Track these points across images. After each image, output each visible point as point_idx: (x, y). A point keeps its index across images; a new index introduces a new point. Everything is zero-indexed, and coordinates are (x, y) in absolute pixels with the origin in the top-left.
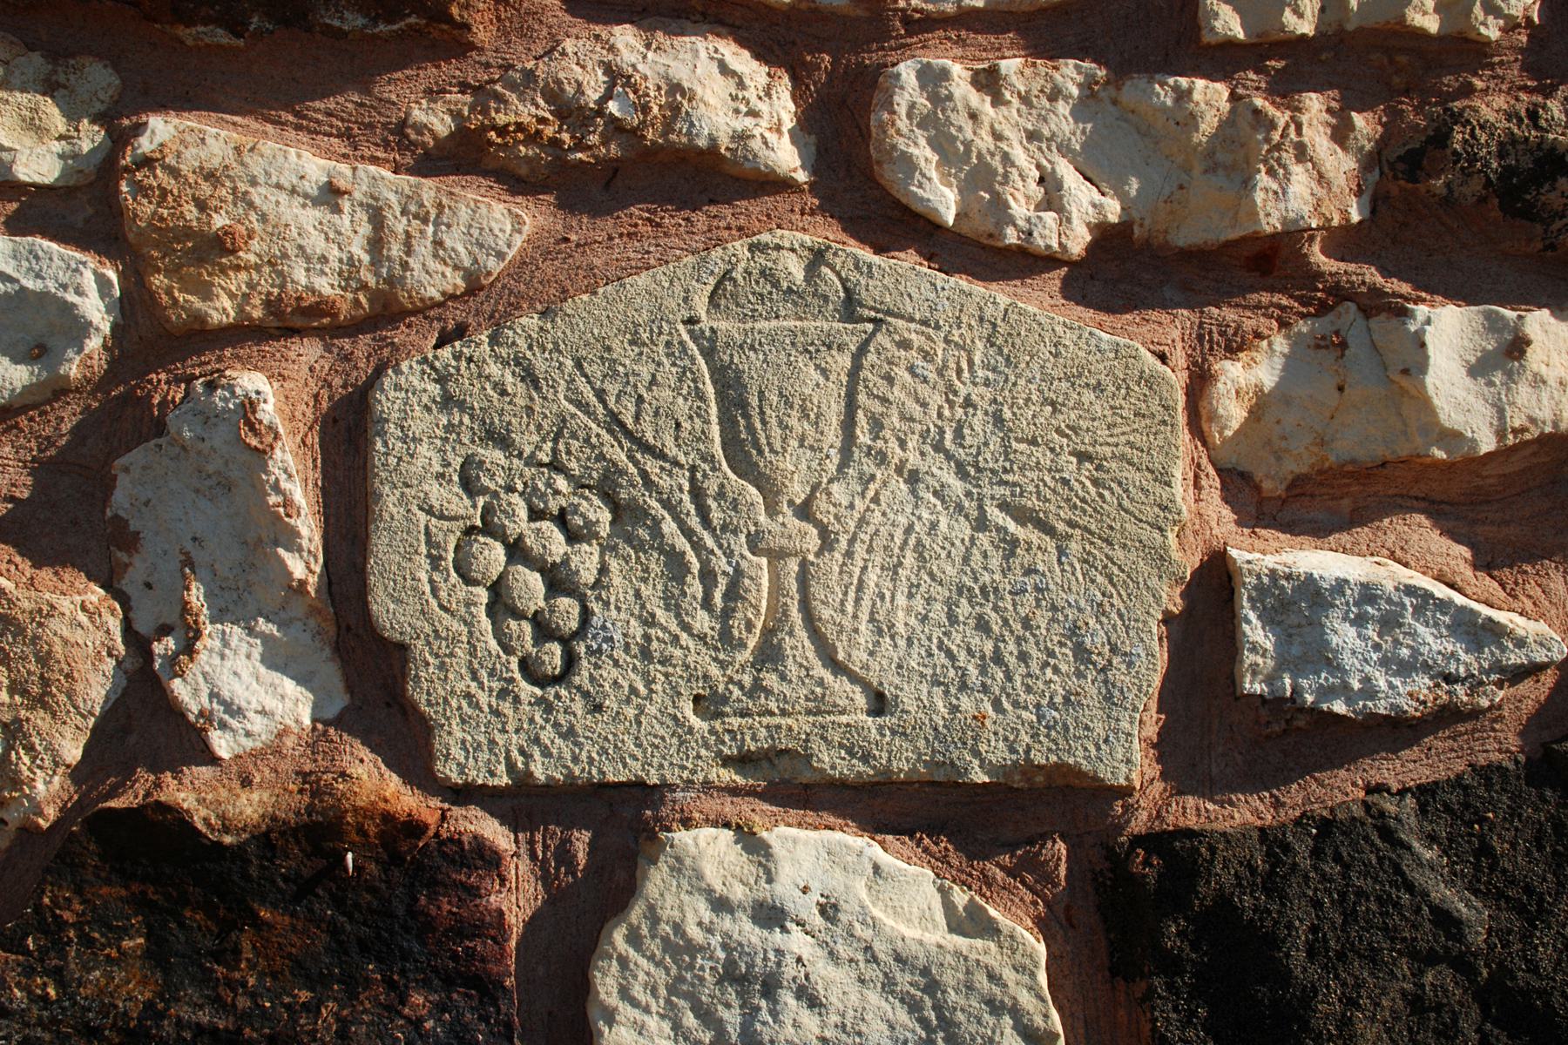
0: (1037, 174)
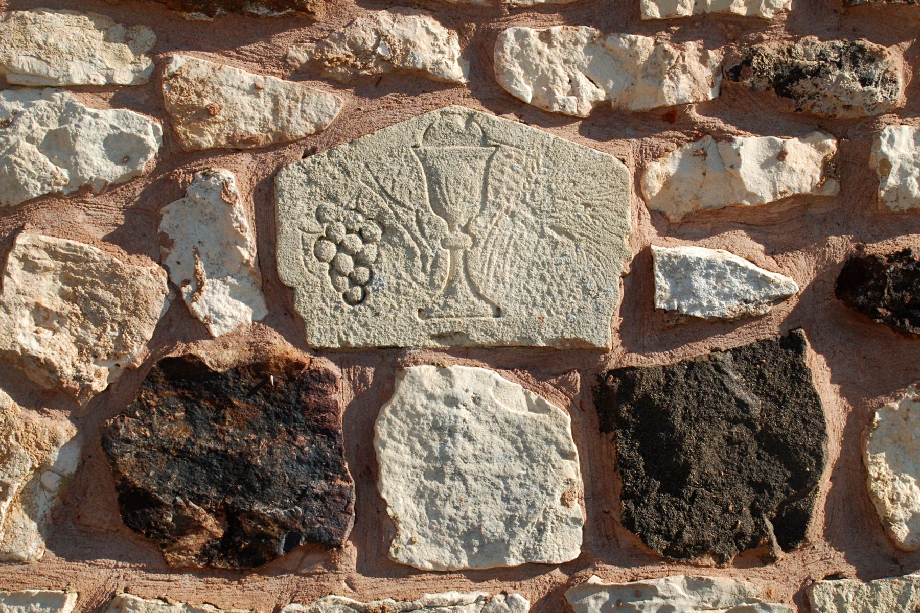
0: (568, 79)
